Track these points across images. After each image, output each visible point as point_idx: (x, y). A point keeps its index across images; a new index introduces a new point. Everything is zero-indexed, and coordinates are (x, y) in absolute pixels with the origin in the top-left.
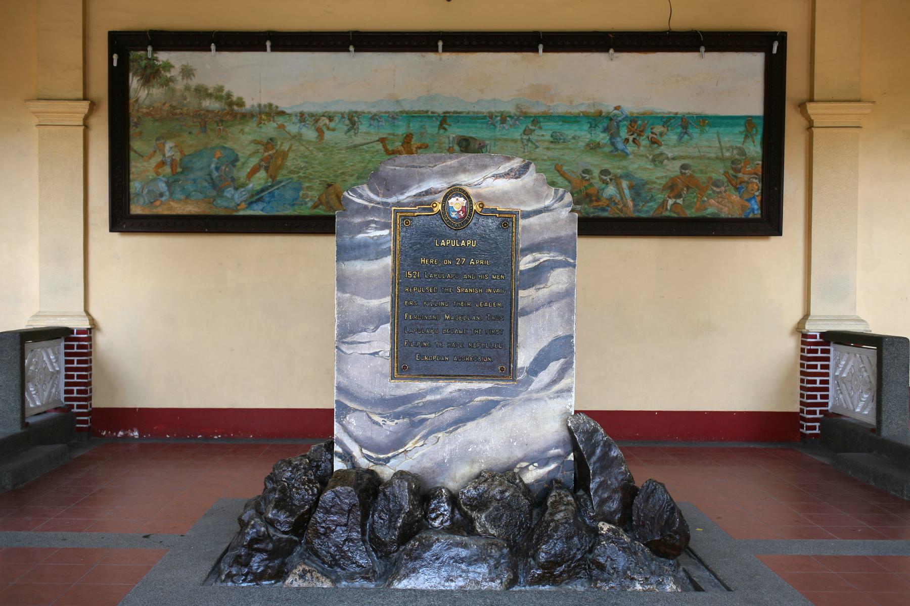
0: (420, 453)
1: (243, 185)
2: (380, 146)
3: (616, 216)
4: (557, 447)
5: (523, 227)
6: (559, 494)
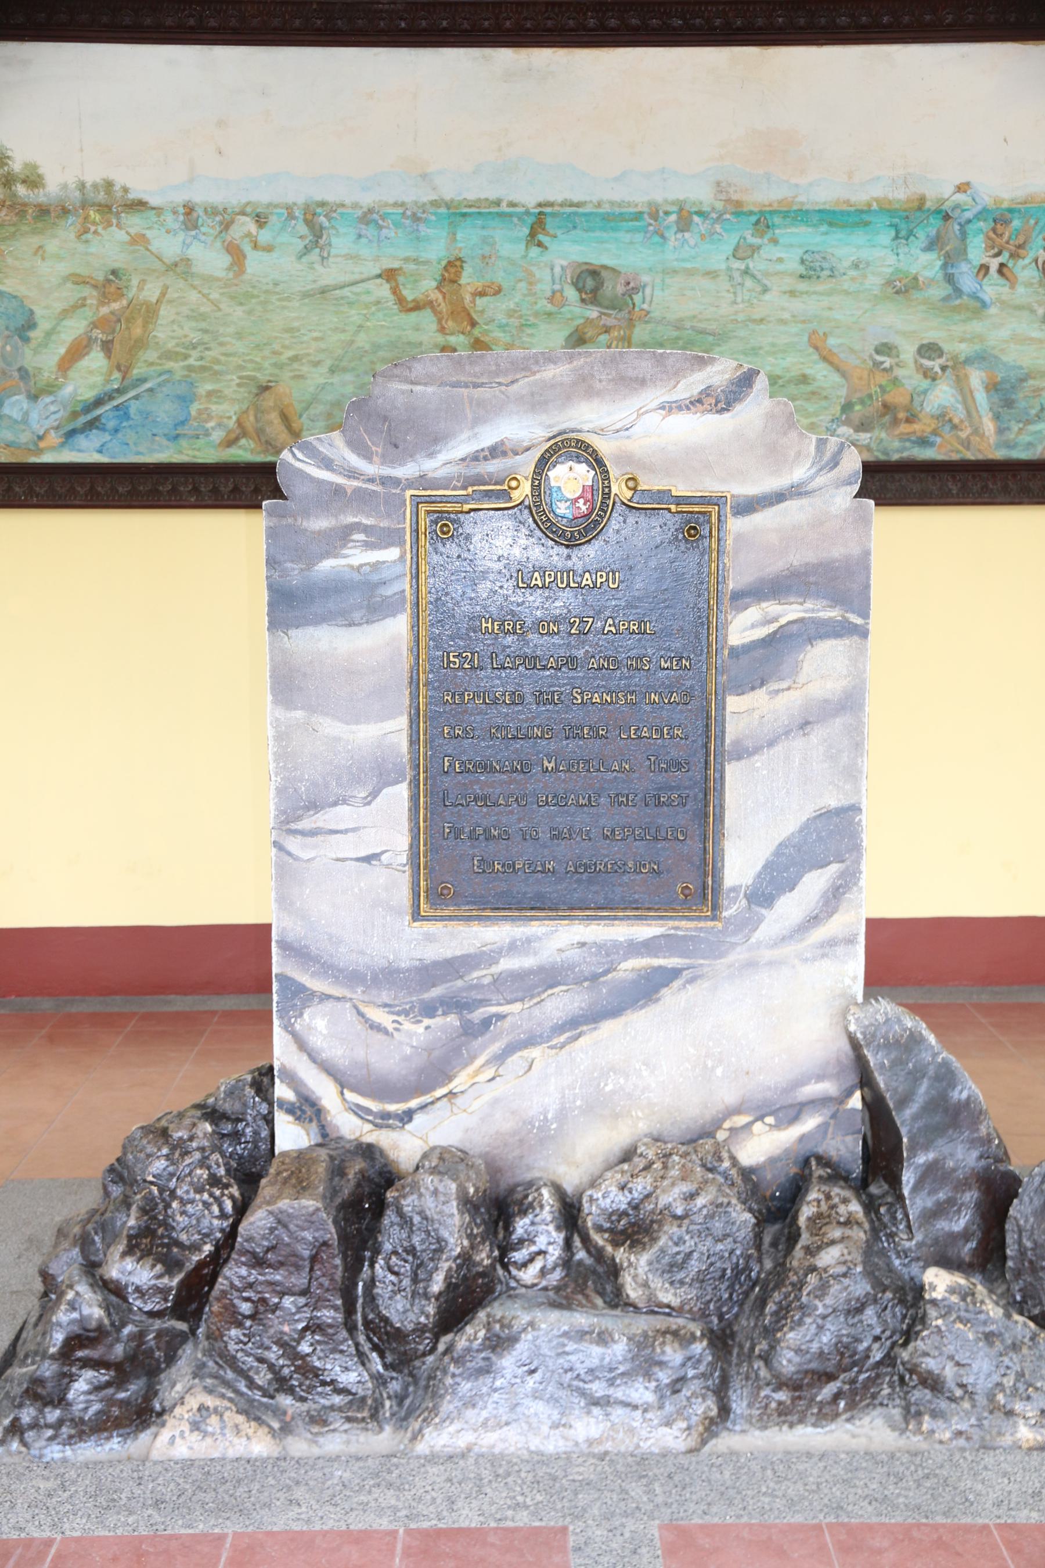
0: (486, 1098)
2: (383, 290)
3: (955, 457)
4: (820, 1078)
5: (739, 537)
6: (828, 1197)
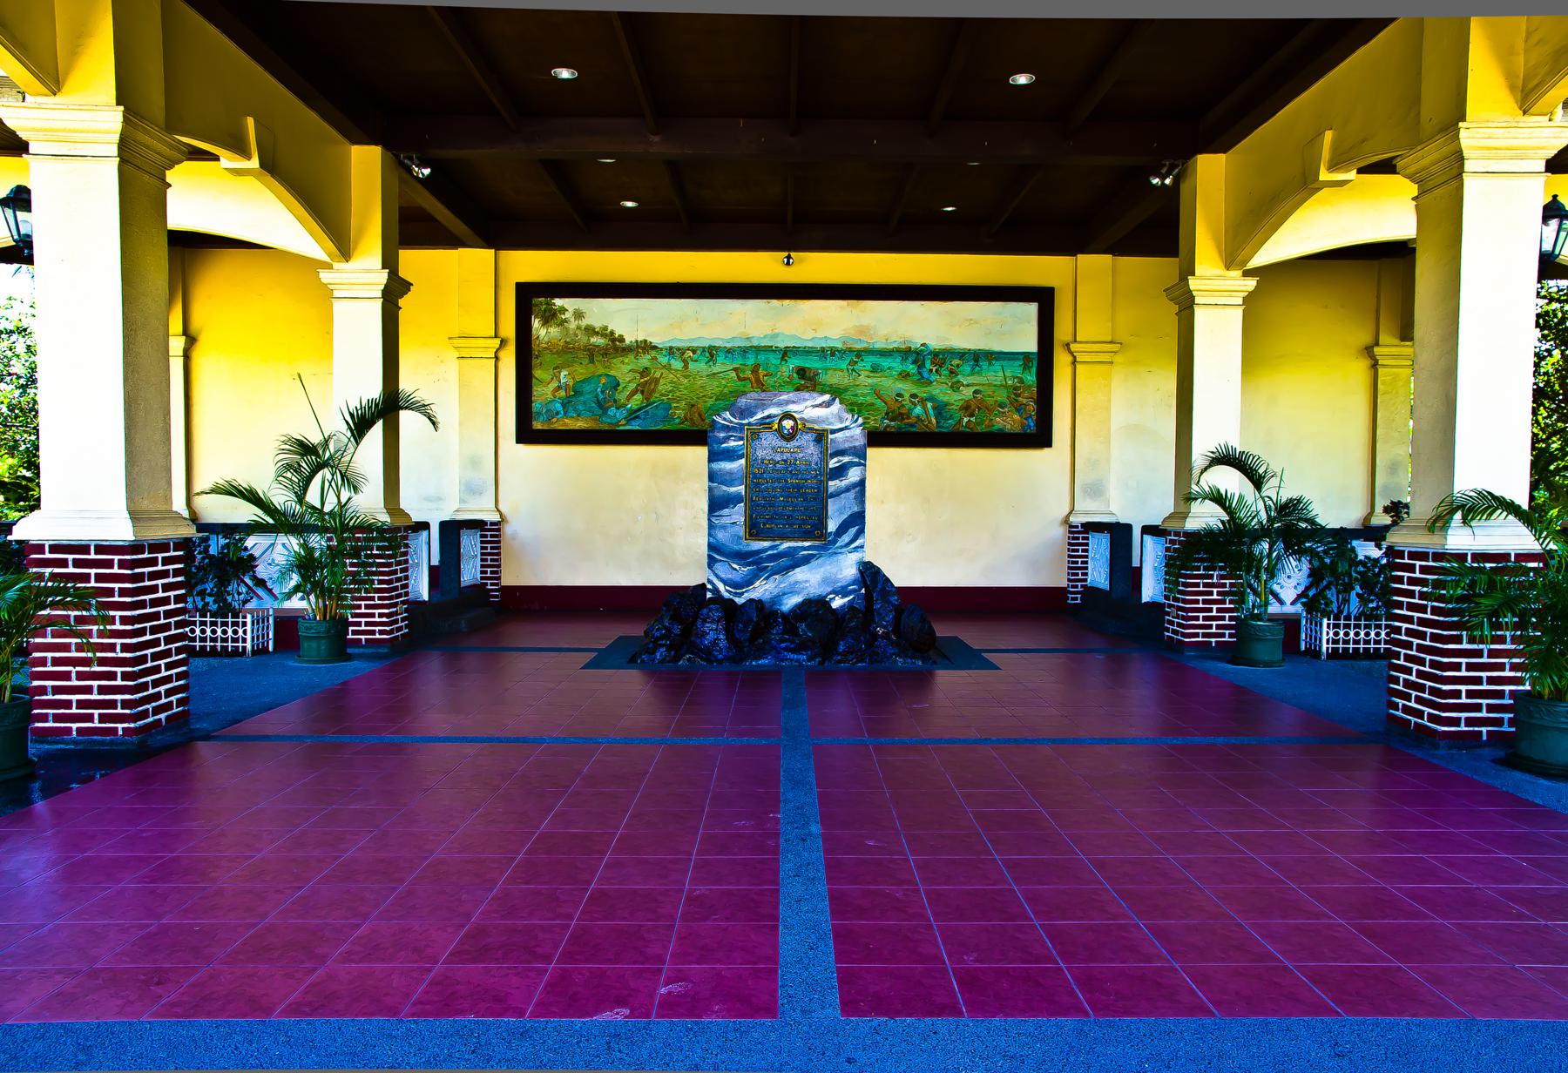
1: (624, 405)
